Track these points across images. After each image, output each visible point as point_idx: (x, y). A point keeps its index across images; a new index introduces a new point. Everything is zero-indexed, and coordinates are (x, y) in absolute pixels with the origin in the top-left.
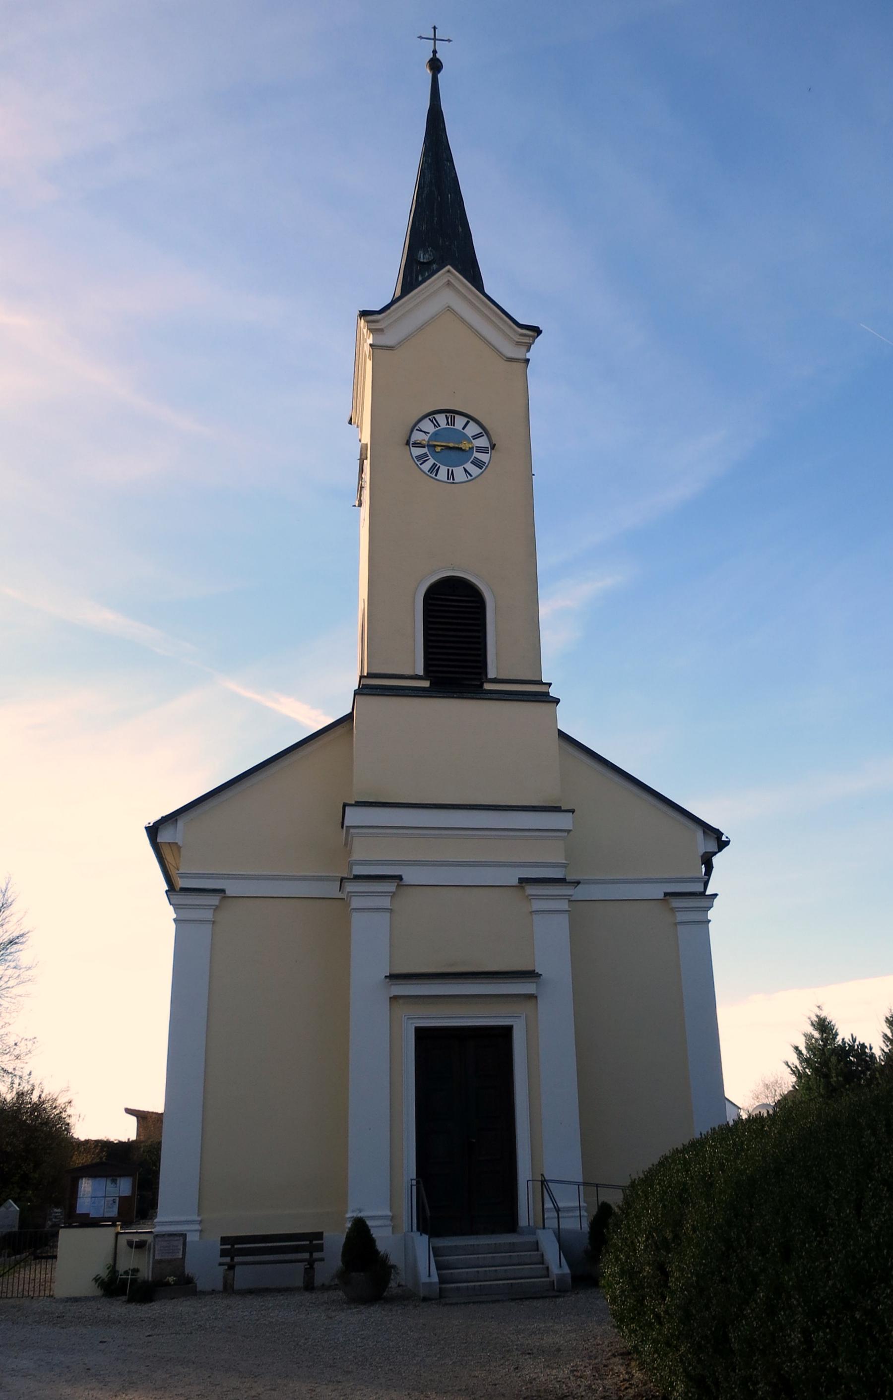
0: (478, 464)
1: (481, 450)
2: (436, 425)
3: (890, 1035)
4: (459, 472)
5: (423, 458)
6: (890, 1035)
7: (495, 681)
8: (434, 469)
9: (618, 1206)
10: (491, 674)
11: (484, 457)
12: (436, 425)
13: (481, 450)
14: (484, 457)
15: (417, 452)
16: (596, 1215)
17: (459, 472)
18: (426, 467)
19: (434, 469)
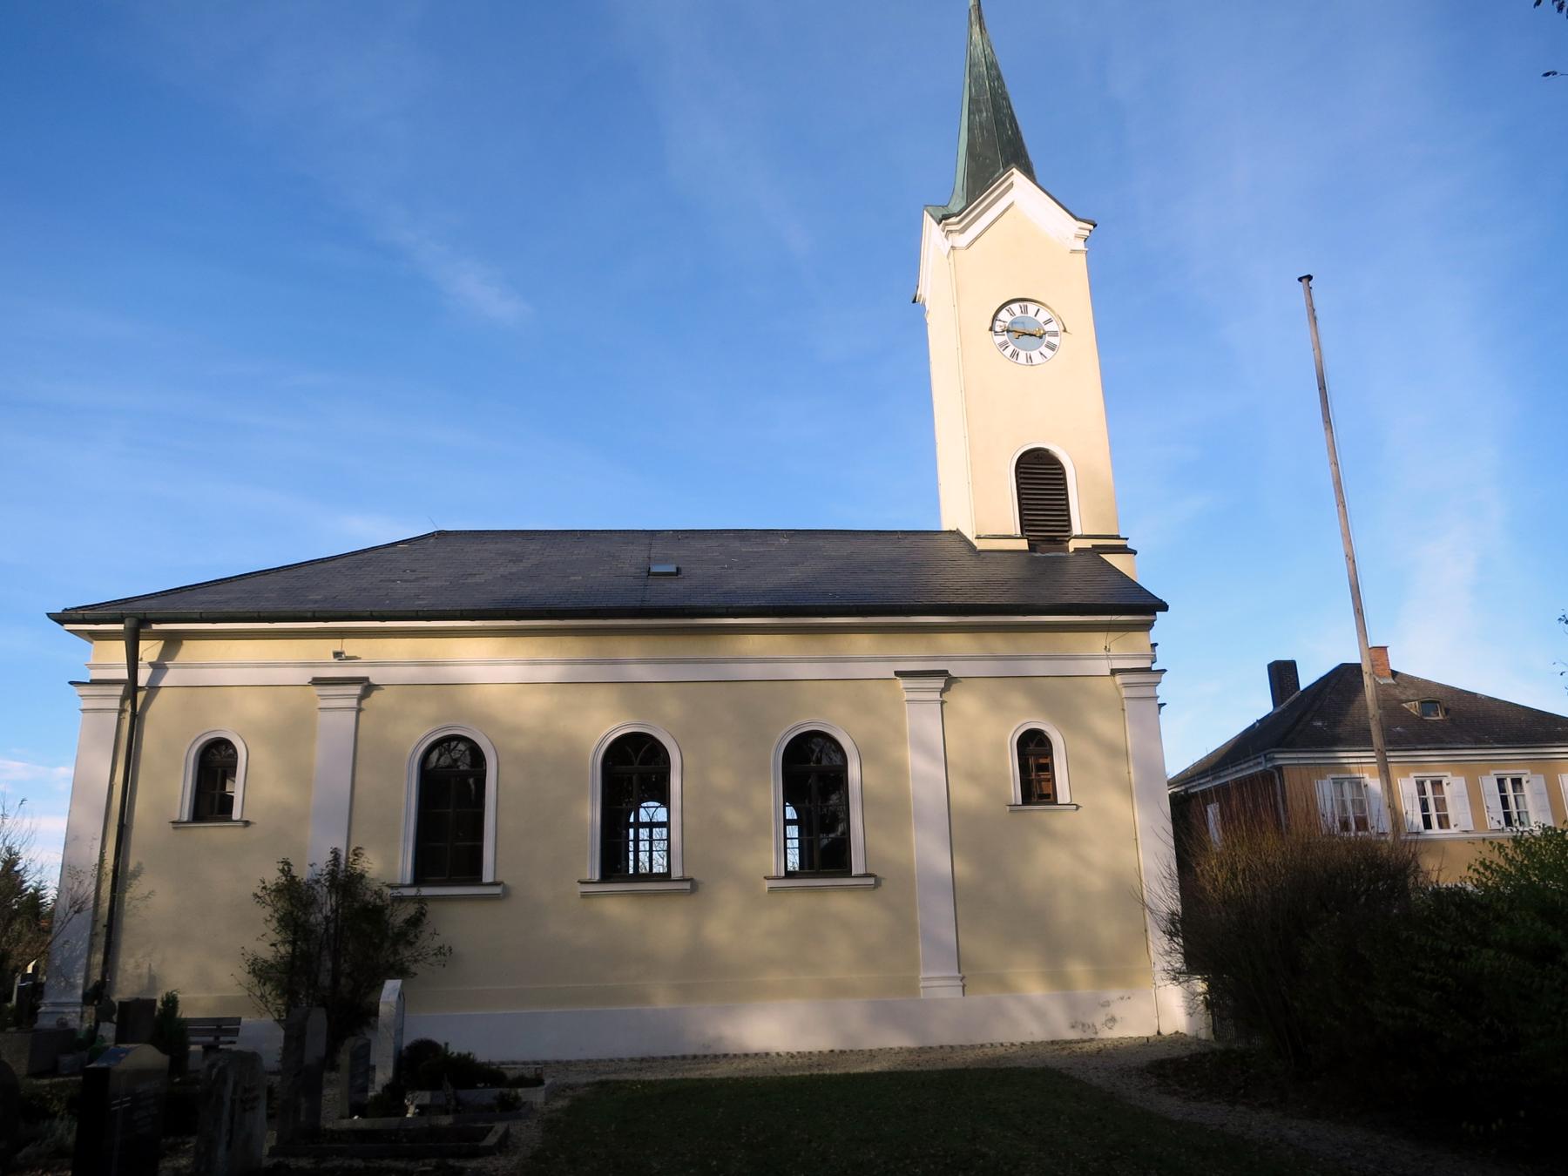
0: (1052, 347)
1: (1055, 334)
2: (1012, 314)
3: (1114, 560)
4: (1035, 355)
5: (1004, 346)
6: (1114, 560)
7: (1076, 537)
8: (1015, 354)
9: (127, 1052)
10: (1076, 530)
11: (1054, 340)
12: (1012, 314)
13: (1055, 334)
14: (1054, 340)
15: (1000, 339)
16: (473, 1061)
17: (1035, 355)
18: (1008, 352)
19: (1015, 354)
